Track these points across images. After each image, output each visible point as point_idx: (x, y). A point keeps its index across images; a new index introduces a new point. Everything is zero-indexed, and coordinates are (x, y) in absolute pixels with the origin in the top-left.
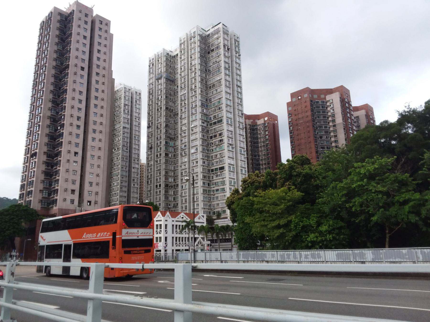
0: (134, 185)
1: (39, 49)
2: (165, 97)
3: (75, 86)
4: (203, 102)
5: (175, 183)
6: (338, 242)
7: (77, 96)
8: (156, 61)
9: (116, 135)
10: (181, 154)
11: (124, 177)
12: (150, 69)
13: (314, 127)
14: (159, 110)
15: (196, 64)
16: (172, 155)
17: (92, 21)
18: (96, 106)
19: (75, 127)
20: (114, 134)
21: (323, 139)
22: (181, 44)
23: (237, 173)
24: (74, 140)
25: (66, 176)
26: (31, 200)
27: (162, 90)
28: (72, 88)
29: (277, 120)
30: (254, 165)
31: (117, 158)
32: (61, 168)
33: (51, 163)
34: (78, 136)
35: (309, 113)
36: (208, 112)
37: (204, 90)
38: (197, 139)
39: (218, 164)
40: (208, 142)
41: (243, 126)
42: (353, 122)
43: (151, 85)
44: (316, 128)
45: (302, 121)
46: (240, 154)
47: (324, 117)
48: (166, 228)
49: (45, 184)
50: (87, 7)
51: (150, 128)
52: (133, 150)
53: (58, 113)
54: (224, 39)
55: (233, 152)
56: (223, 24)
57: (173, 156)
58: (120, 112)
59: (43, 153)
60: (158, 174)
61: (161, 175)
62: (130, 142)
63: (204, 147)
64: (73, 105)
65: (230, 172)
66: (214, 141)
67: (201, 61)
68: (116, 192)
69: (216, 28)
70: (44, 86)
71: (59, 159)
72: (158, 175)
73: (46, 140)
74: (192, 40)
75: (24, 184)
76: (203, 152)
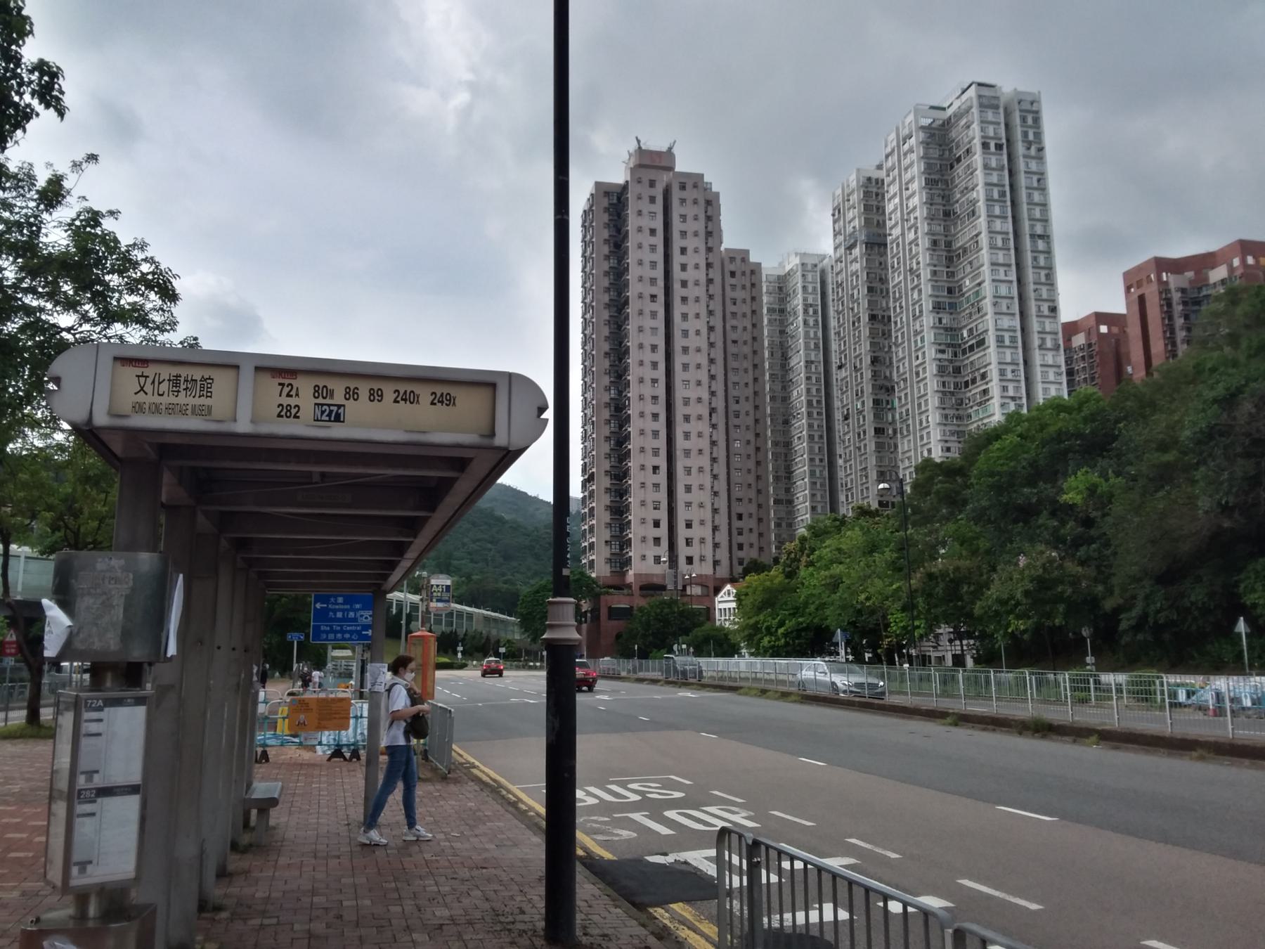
4: (939, 300)
12: (835, 222)
20: (791, 380)
26: (593, 560)
28: (636, 343)
51: (843, 369)
58: (797, 327)
59: (603, 473)
61: (868, 482)
63: (947, 412)
64: (641, 376)
66: (973, 392)
68: (804, 517)
69: (964, 97)
76: (945, 425)
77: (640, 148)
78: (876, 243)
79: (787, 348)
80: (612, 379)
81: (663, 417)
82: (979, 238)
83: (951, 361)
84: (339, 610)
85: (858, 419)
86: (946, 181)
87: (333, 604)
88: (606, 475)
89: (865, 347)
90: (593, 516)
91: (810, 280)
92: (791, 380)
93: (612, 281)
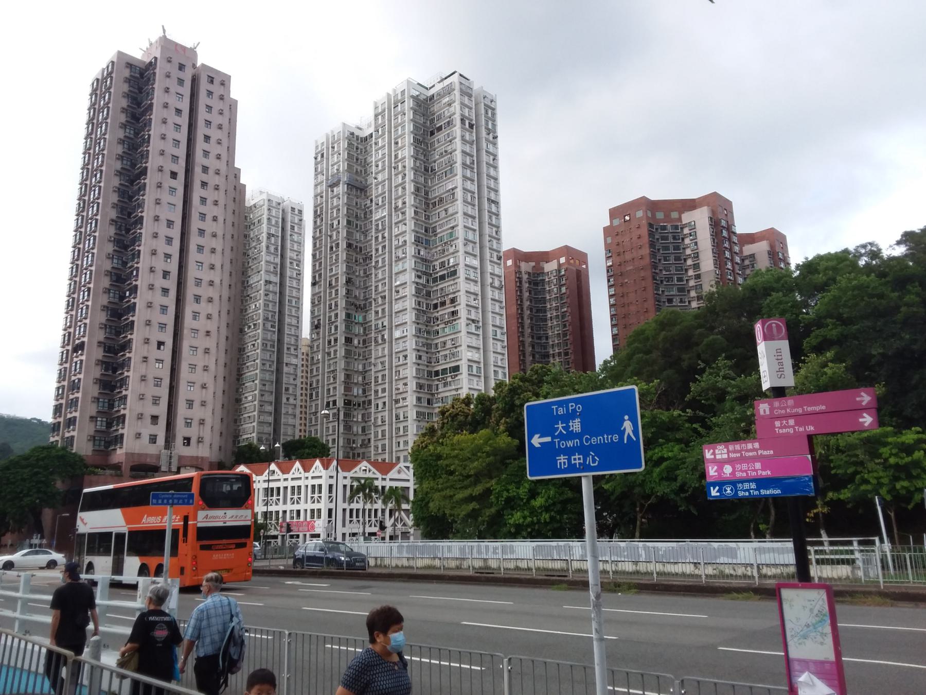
0: (288, 399)
1: (88, 136)
2: (345, 224)
3: (159, 211)
5: (366, 397)
6: (559, 525)
7: (163, 231)
8: (328, 148)
9: (251, 298)
10: (376, 341)
11: (267, 384)
12: (316, 164)
13: (656, 280)
14: (334, 249)
15: (405, 158)
16: (359, 341)
17: (193, 76)
18: (200, 248)
19: (159, 292)
20: (248, 296)
21: (674, 304)
22: (376, 116)
23: (486, 378)
24: (157, 317)
25: (141, 388)
26: (73, 437)
27: (341, 207)
28: (152, 214)
29: (586, 263)
30: (537, 356)
31: (254, 345)
32: (130, 374)
33: (113, 363)
34: (164, 309)
35: (646, 251)
36: (430, 255)
37: (422, 209)
38: (406, 309)
39: (448, 360)
40: (429, 315)
41: (501, 282)
42: (737, 267)
43: (319, 197)
44: (659, 282)
45: (631, 268)
46: (493, 339)
47: (677, 259)
48: (330, 491)
49: (101, 404)
50: (184, 48)
51: (317, 286)
52: (286, 329)
53: (127, 263)
54: (463, 104)
55: (478, 335)
56: (461, 75)
57: (361, 342)
58: (260, 252)
60: (332, 379)
62: (280, 312)
63: (420, 326)
65: (471, 378)
66: (440, 313)
67: (416, 152)
68: (250, 414)
70: (98, 210)
71: (128, 355)
72: (332, 380)
73: (102, 317)
74: (399, 108)
75: (61, 405)
76: (418, 337)
77: (165, 37)
79: (247, 268)
82: (455, 191)
88: (99, 346)
89: (342, 268)
91: (274, 215)
92: (248, 296)
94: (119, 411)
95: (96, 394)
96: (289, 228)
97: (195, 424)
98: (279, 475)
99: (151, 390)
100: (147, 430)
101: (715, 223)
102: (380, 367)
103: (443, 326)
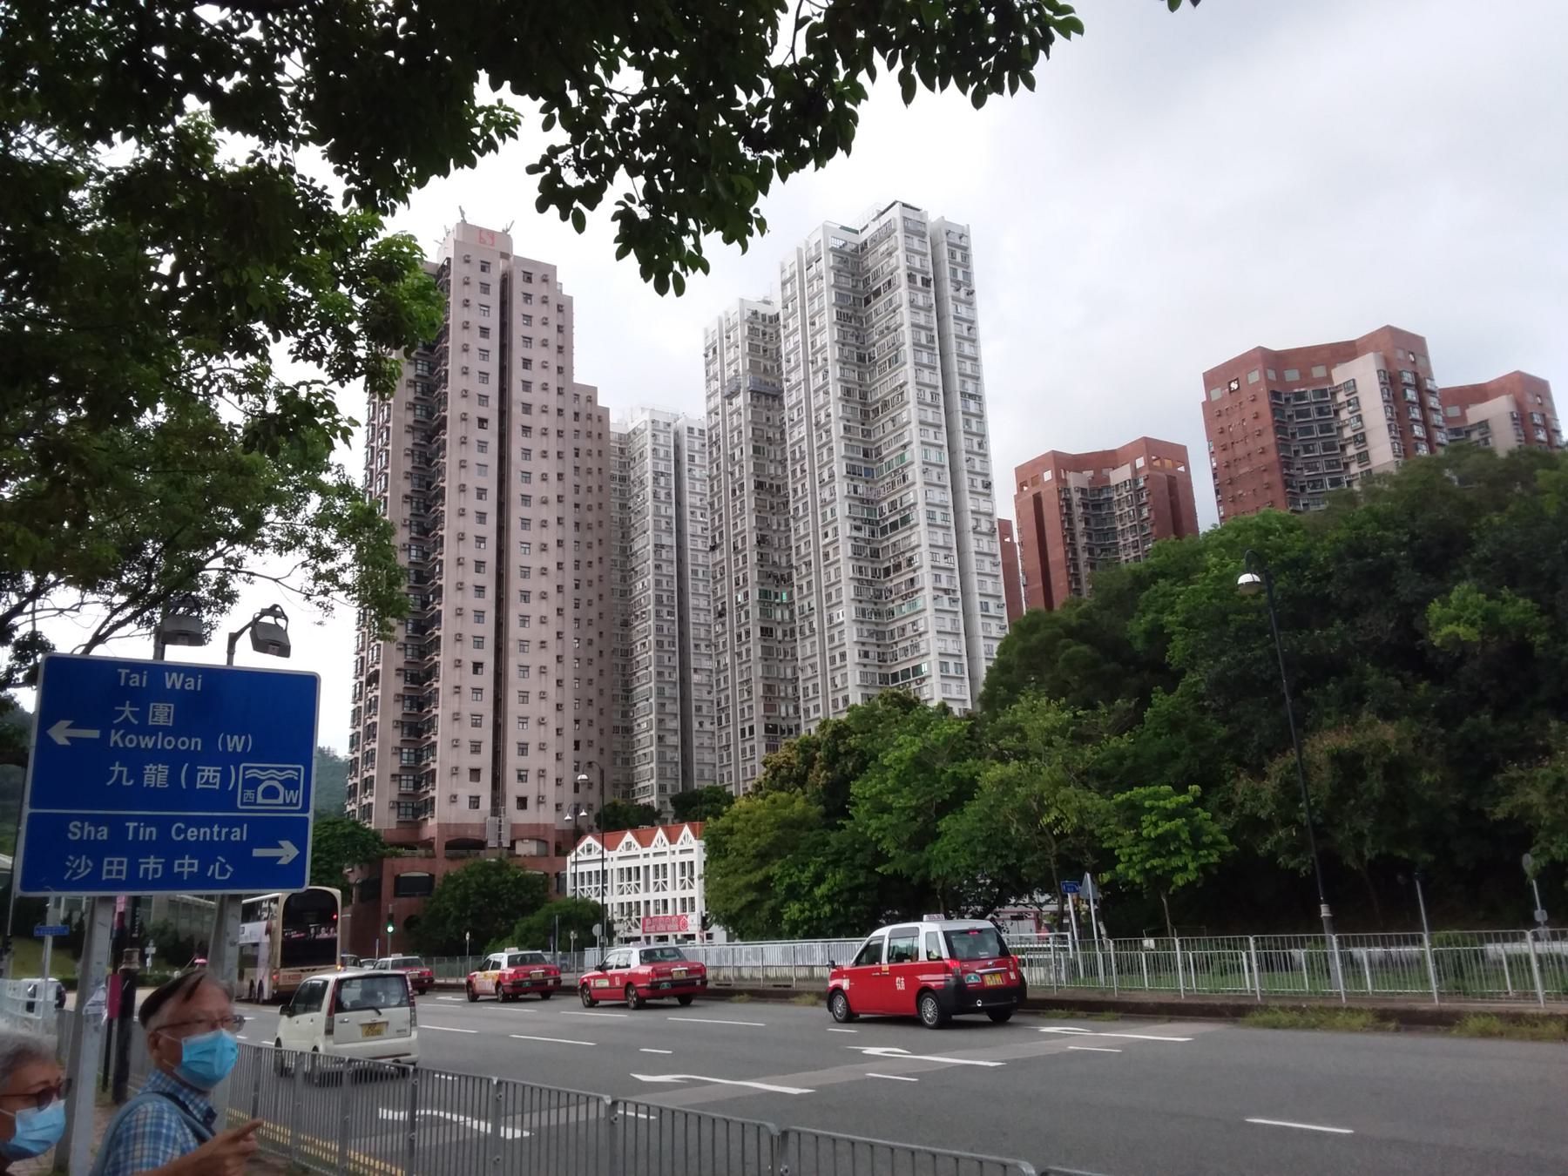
0: (701, 724)
4: (853, 463)
8: (721, 339)
10: (802, 633)
12: (707, 364)
19: (471, 592)
26: (370, 805)
28: (455, 484)
31: (644, 644)
35: (1269, 439)
39: (910, 656)
44: (1298, 491)
45: (1247, 469)
47: (1329, 447)
49: (405, 756)
50: (492, 234)
51: (718, 552)
53: (429, 554)
58: (644, 501)
59: (394, 672)
63: (864, 605)
65: (947, 681)
66: (895, 582)
68: (646, 751)
69: (884, 219)
72: (746, 697)
76: (862, 622)
77: (464, 221)
78: (767, 394)
80: (414, 535)
81: (491, 592)
82: (905, 388)
83: (868, 542)
84: (156, 756)
85: (739, 616)
86: (860, 319)
87: (127, 727)
90: (375, 736)
91: (662, 442)
93: (419, 395)
94: (428, 765)
95: (398, 743)
96: (686, 459)
97: (532, 777)
98: (637, 849)
99: (468, 734)
100: (466, 789)
101: (1391, 382)
102: (809, 672)
103: (900, 602)
